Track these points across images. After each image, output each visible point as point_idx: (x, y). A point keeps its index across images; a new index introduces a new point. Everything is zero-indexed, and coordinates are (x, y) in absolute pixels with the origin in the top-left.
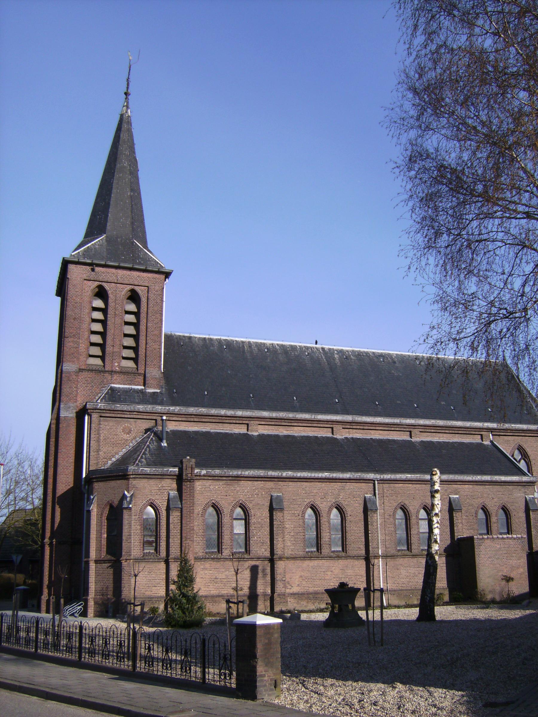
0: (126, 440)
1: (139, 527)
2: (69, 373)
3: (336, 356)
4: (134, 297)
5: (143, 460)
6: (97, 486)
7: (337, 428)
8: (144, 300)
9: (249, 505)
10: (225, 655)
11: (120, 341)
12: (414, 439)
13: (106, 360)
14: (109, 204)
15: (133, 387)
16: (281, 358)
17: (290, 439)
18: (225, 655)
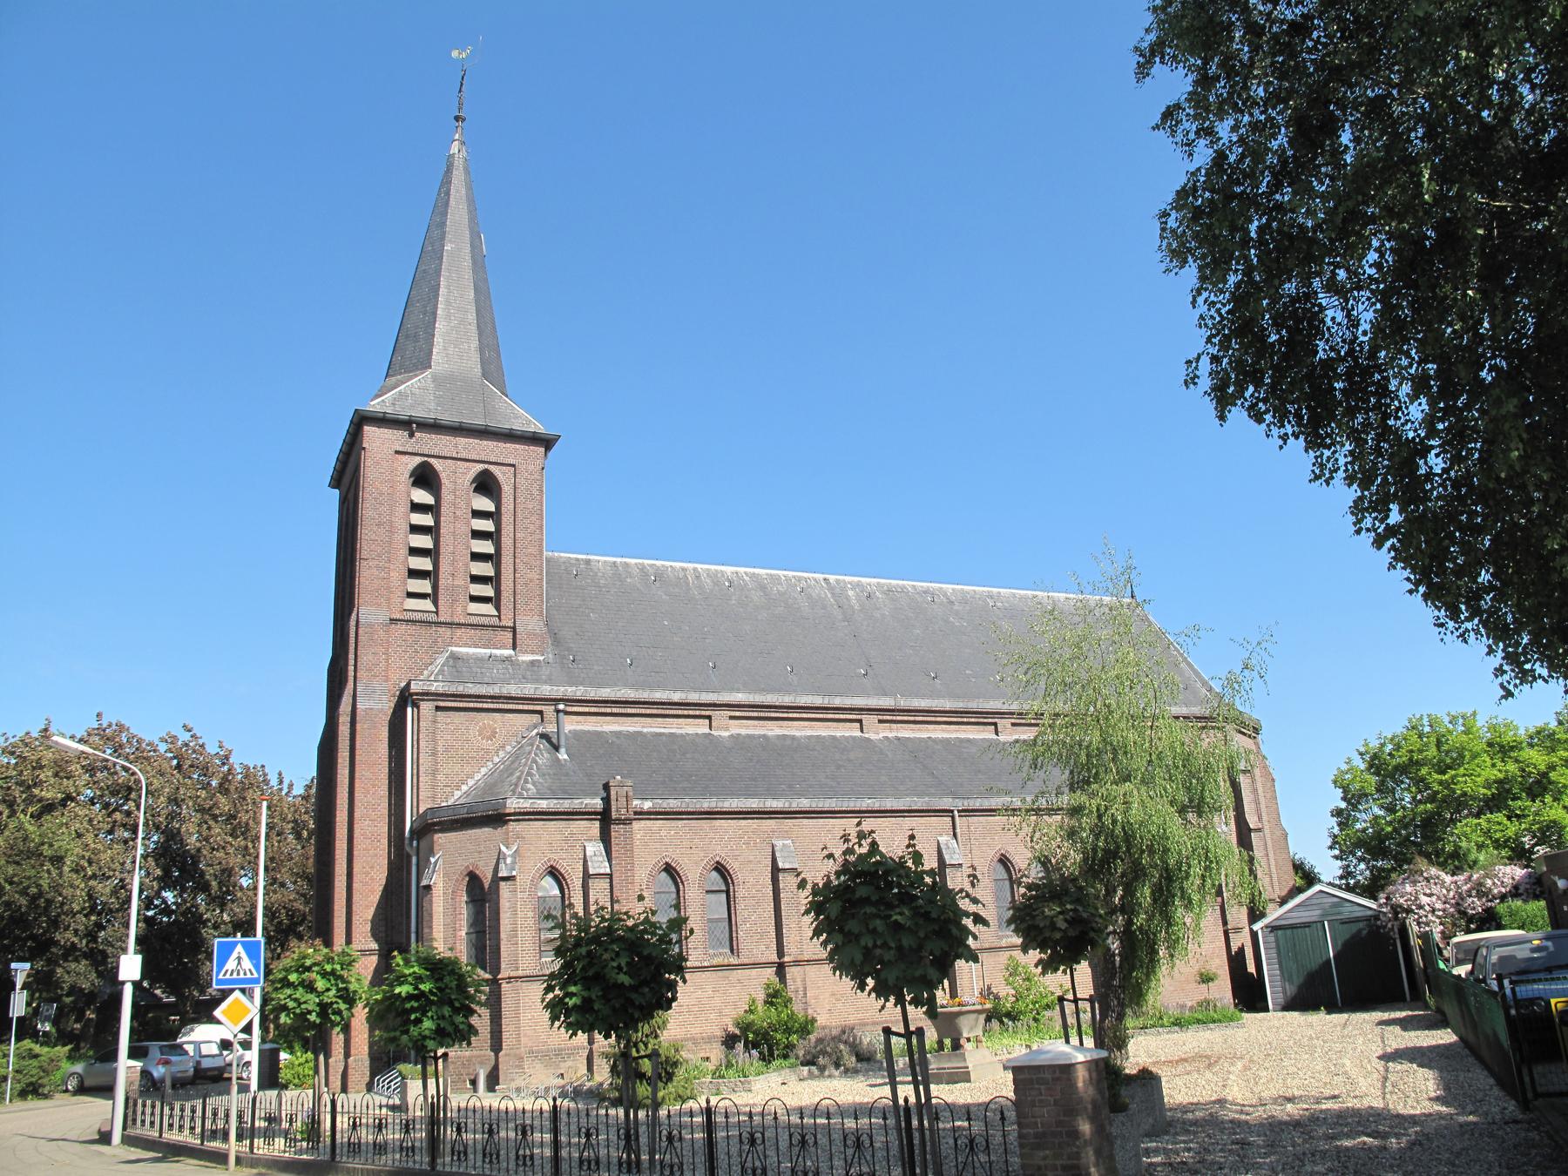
0: (487, 751)
1: (531, 914)
2: (371, 625)
3: (851, 593)
4: (486, 484)
5: (529, 786)
6: (440, 838)
7: (720, 716)
8: (507, 490)
9: (733, 866)
10: (752, 1135)
11: (467, 565)
12: (1002, 738)
13: (441, 602)
14: (435, 314)
15: (495, 652)
16: (756, 596)
17: (789, 742)
18: (752, 1135)
